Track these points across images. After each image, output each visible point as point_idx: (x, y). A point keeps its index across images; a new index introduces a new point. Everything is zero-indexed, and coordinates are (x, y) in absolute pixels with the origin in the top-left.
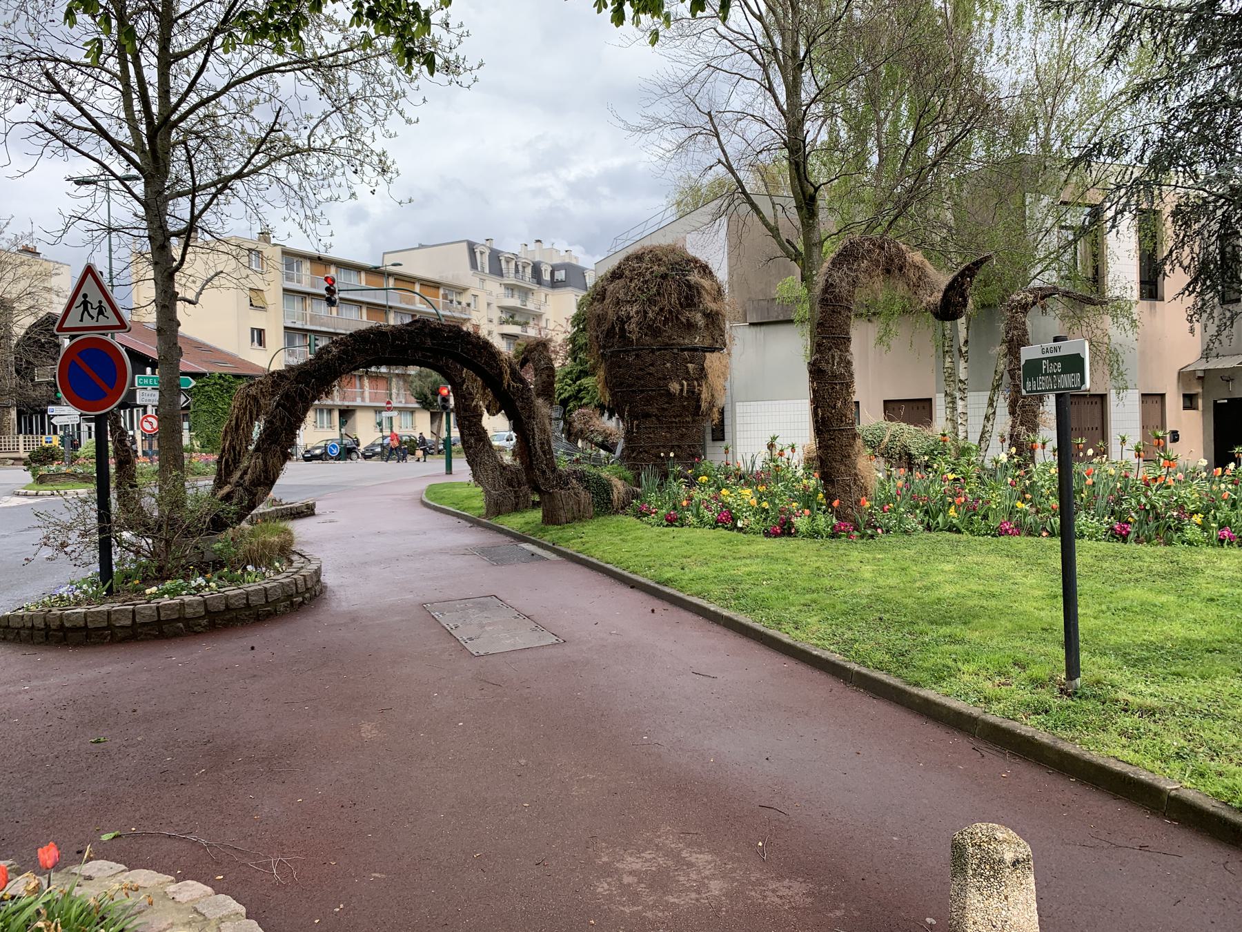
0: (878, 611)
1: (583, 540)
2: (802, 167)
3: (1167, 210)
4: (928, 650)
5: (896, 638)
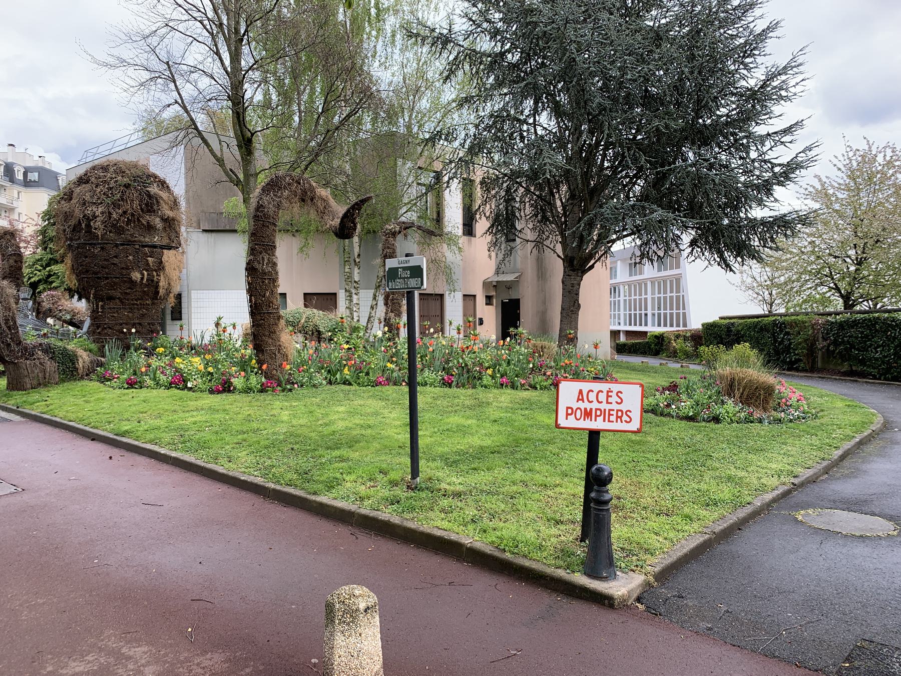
0: (291, 443)
1: (48, 403)
2: (241, 116)
3: (478, 180)
4: (324, 468)
5: (303, 462)
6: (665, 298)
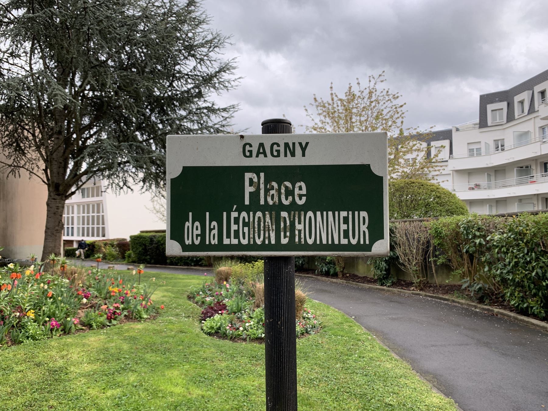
6: (88, 217)
